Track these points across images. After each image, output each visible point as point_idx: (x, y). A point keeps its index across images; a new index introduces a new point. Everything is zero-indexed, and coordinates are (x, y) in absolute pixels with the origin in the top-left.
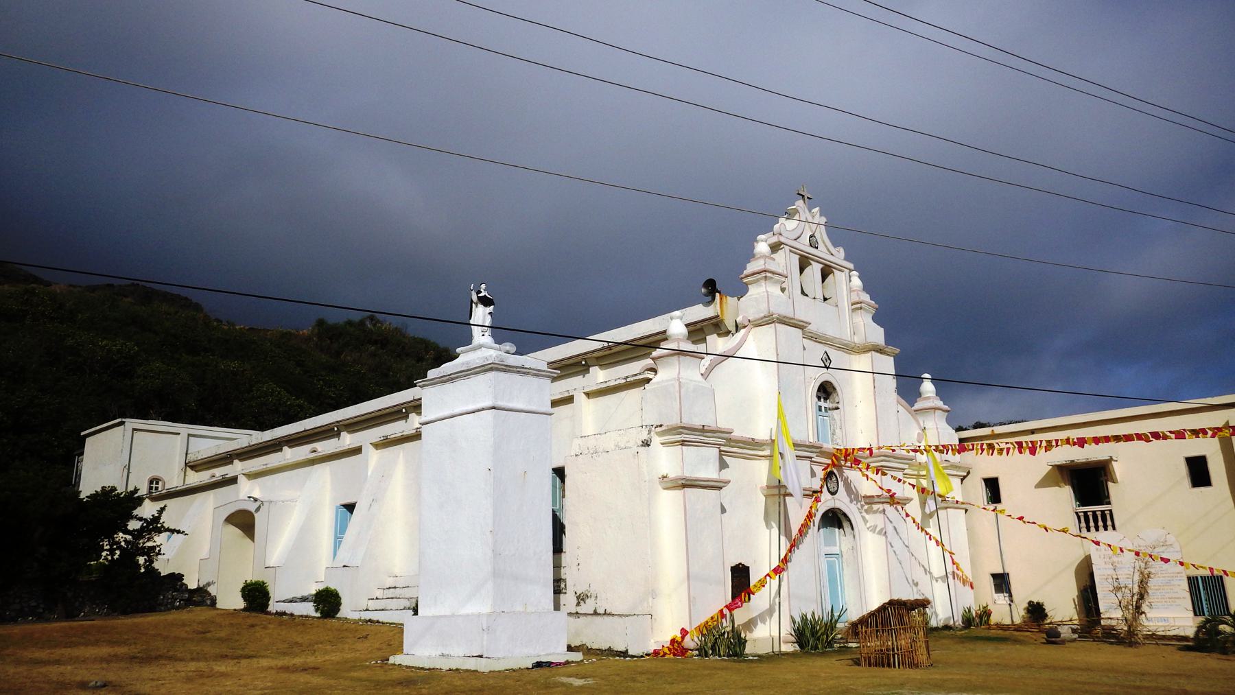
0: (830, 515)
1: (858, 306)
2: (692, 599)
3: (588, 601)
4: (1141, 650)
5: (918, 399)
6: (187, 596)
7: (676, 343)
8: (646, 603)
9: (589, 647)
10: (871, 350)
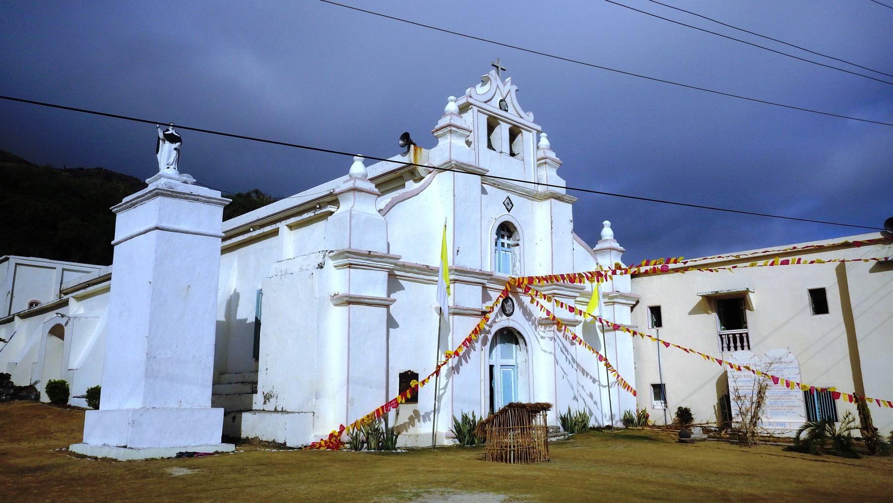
0: (505, 333)
1: (543, 161)
2: (350, 399)
3: (271, 400)
4: (753, 449)
5: (599, 242)
6: (12, 391)
7: (353, 181)
8: (310, 403)
9: (261, 440)
10: (550, 198)
